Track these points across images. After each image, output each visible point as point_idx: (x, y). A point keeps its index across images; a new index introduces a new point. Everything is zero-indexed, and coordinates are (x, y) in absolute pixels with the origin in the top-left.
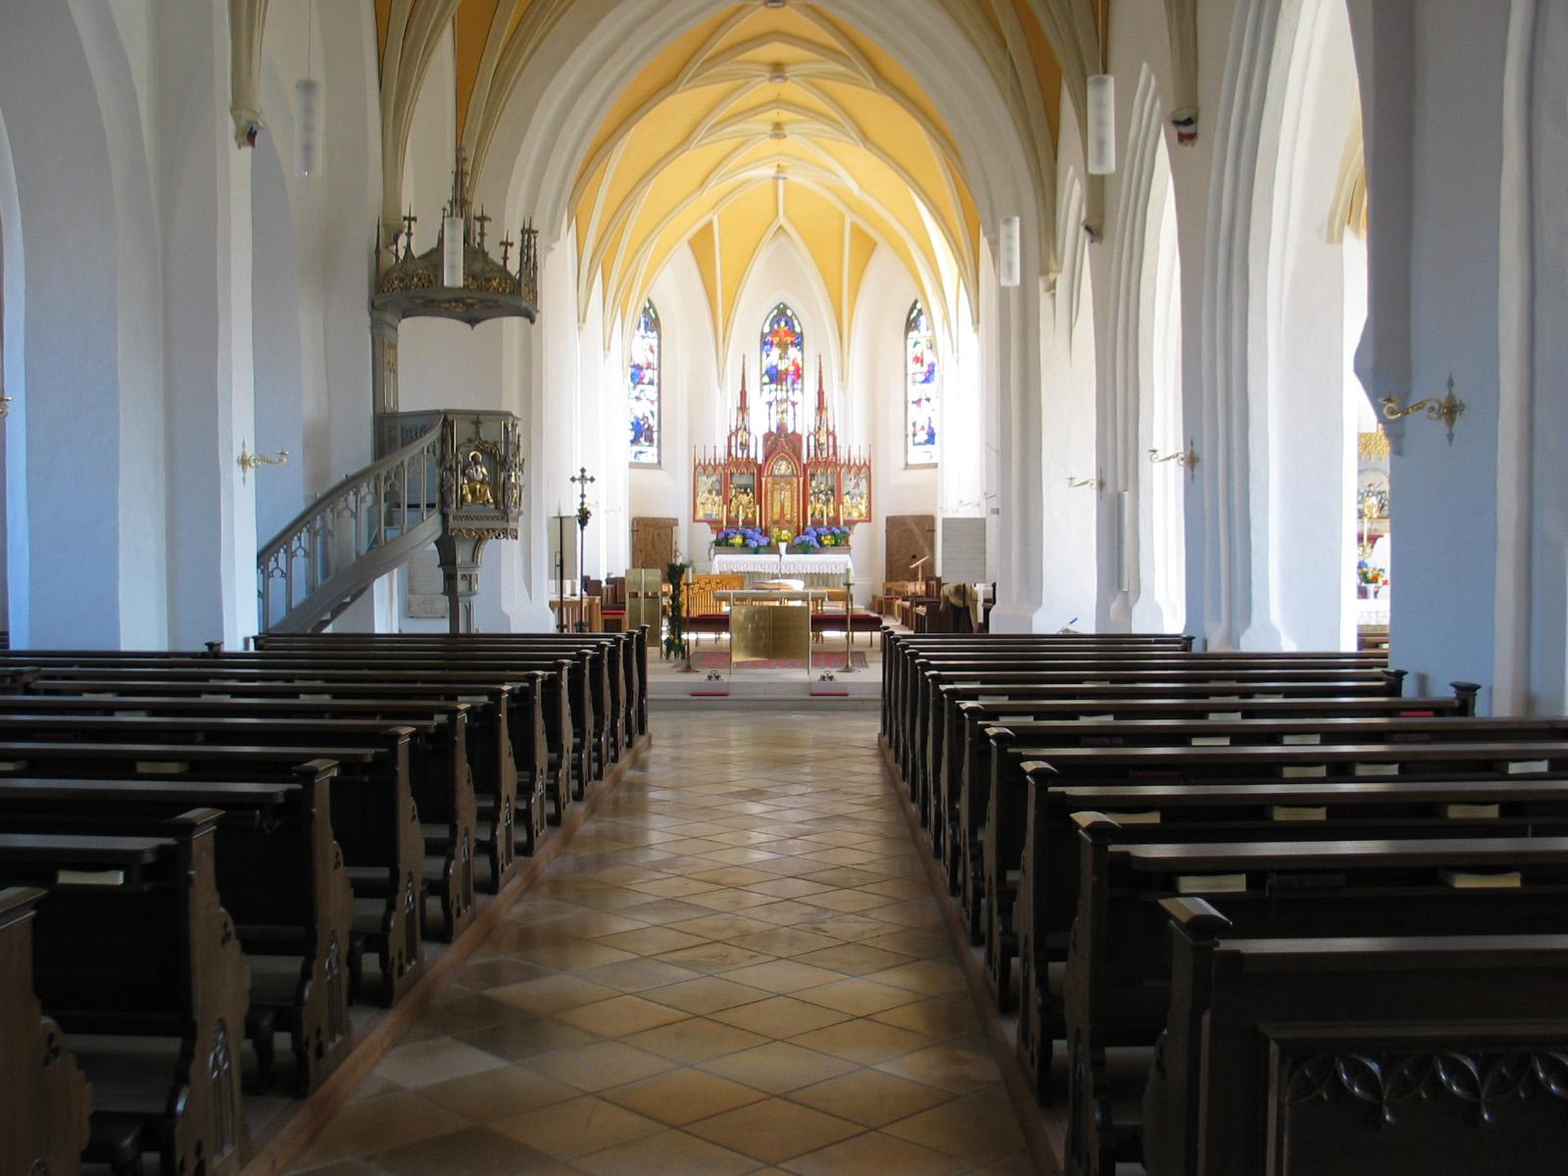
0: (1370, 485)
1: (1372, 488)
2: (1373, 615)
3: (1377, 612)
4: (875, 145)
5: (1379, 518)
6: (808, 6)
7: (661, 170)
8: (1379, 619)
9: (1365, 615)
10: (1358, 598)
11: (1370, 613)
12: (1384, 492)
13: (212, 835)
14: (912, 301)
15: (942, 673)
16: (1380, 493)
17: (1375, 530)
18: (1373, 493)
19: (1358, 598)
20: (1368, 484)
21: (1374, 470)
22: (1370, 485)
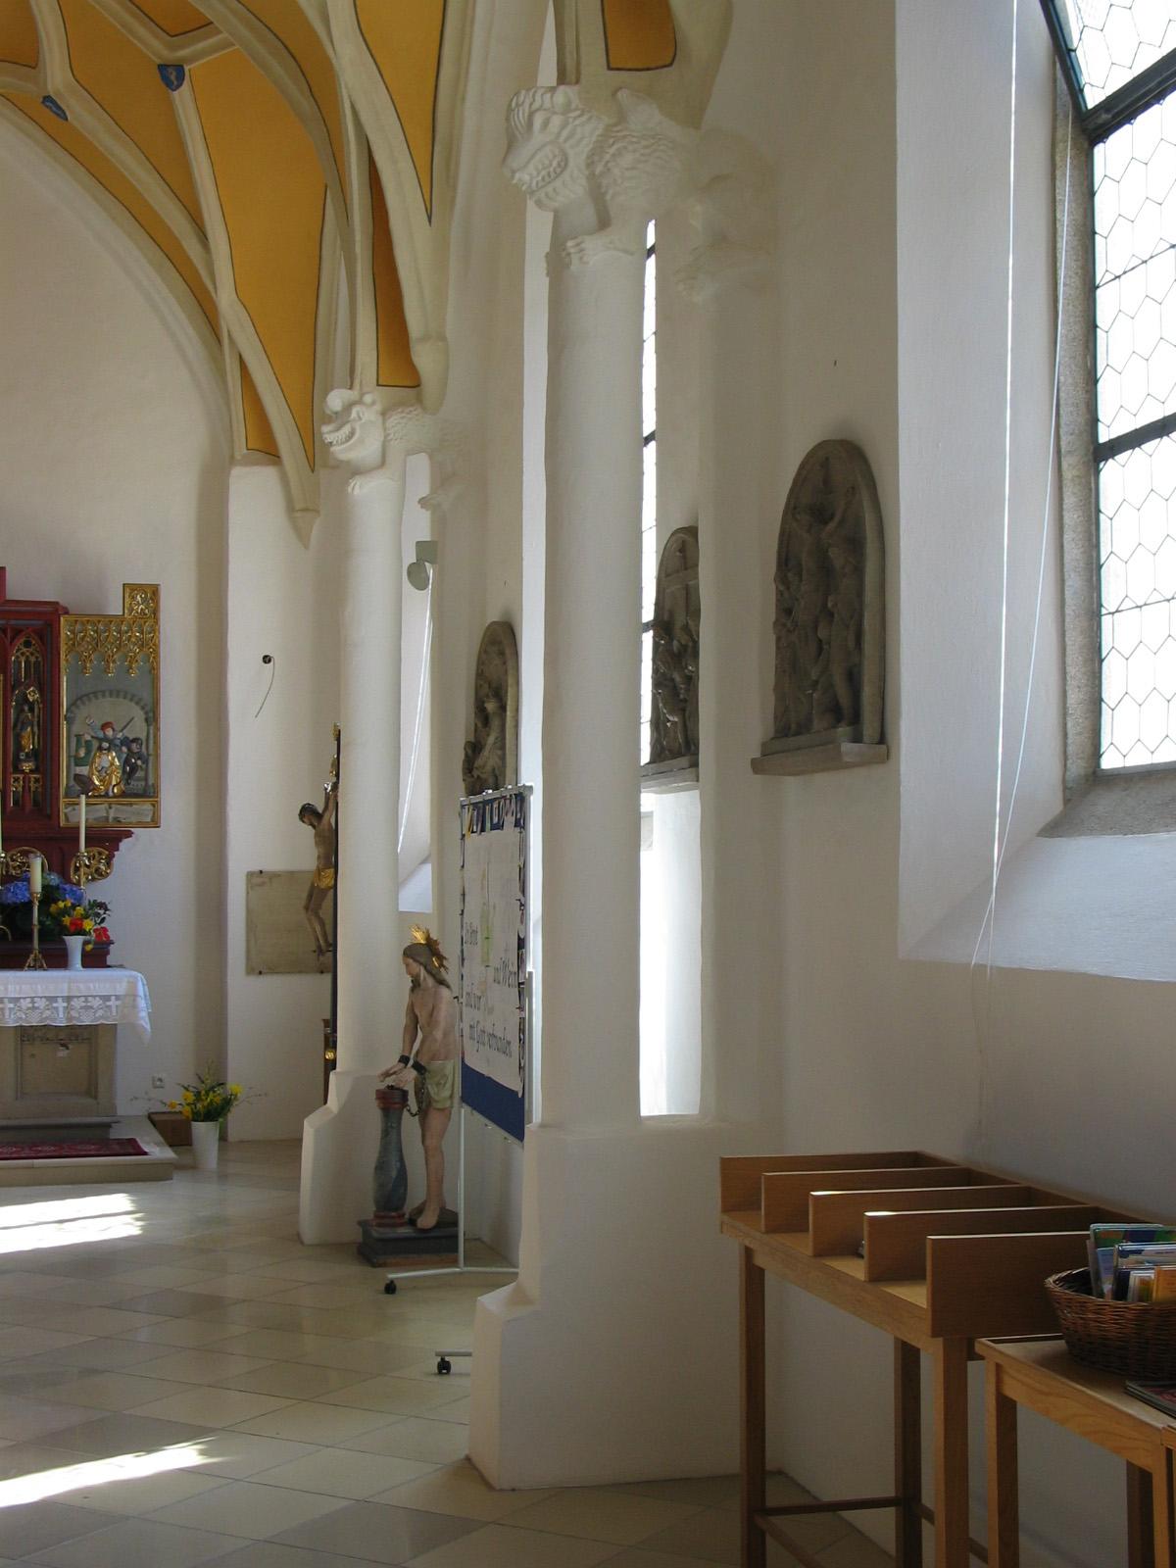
0: (104, 726)
1: (109, 733)
2: (61, 1004)
3: (68, 999)
4: (115, 966)
5: (123, 794)
6: (522, 922)
7: (465, 86)
8: (74, 1014)
9: (41, 1004)
10: (377, 1091)
11: (52, 999)
12: (135, 740)
13: (512, 1082)
14: (700, 779)
15: (648, 614)
16: (126, 742)
17: (117, 820)
18: (110, 741)
19: (377, 1091)
20: (99, 724)
21: (115, 693)
22: (104, 726)
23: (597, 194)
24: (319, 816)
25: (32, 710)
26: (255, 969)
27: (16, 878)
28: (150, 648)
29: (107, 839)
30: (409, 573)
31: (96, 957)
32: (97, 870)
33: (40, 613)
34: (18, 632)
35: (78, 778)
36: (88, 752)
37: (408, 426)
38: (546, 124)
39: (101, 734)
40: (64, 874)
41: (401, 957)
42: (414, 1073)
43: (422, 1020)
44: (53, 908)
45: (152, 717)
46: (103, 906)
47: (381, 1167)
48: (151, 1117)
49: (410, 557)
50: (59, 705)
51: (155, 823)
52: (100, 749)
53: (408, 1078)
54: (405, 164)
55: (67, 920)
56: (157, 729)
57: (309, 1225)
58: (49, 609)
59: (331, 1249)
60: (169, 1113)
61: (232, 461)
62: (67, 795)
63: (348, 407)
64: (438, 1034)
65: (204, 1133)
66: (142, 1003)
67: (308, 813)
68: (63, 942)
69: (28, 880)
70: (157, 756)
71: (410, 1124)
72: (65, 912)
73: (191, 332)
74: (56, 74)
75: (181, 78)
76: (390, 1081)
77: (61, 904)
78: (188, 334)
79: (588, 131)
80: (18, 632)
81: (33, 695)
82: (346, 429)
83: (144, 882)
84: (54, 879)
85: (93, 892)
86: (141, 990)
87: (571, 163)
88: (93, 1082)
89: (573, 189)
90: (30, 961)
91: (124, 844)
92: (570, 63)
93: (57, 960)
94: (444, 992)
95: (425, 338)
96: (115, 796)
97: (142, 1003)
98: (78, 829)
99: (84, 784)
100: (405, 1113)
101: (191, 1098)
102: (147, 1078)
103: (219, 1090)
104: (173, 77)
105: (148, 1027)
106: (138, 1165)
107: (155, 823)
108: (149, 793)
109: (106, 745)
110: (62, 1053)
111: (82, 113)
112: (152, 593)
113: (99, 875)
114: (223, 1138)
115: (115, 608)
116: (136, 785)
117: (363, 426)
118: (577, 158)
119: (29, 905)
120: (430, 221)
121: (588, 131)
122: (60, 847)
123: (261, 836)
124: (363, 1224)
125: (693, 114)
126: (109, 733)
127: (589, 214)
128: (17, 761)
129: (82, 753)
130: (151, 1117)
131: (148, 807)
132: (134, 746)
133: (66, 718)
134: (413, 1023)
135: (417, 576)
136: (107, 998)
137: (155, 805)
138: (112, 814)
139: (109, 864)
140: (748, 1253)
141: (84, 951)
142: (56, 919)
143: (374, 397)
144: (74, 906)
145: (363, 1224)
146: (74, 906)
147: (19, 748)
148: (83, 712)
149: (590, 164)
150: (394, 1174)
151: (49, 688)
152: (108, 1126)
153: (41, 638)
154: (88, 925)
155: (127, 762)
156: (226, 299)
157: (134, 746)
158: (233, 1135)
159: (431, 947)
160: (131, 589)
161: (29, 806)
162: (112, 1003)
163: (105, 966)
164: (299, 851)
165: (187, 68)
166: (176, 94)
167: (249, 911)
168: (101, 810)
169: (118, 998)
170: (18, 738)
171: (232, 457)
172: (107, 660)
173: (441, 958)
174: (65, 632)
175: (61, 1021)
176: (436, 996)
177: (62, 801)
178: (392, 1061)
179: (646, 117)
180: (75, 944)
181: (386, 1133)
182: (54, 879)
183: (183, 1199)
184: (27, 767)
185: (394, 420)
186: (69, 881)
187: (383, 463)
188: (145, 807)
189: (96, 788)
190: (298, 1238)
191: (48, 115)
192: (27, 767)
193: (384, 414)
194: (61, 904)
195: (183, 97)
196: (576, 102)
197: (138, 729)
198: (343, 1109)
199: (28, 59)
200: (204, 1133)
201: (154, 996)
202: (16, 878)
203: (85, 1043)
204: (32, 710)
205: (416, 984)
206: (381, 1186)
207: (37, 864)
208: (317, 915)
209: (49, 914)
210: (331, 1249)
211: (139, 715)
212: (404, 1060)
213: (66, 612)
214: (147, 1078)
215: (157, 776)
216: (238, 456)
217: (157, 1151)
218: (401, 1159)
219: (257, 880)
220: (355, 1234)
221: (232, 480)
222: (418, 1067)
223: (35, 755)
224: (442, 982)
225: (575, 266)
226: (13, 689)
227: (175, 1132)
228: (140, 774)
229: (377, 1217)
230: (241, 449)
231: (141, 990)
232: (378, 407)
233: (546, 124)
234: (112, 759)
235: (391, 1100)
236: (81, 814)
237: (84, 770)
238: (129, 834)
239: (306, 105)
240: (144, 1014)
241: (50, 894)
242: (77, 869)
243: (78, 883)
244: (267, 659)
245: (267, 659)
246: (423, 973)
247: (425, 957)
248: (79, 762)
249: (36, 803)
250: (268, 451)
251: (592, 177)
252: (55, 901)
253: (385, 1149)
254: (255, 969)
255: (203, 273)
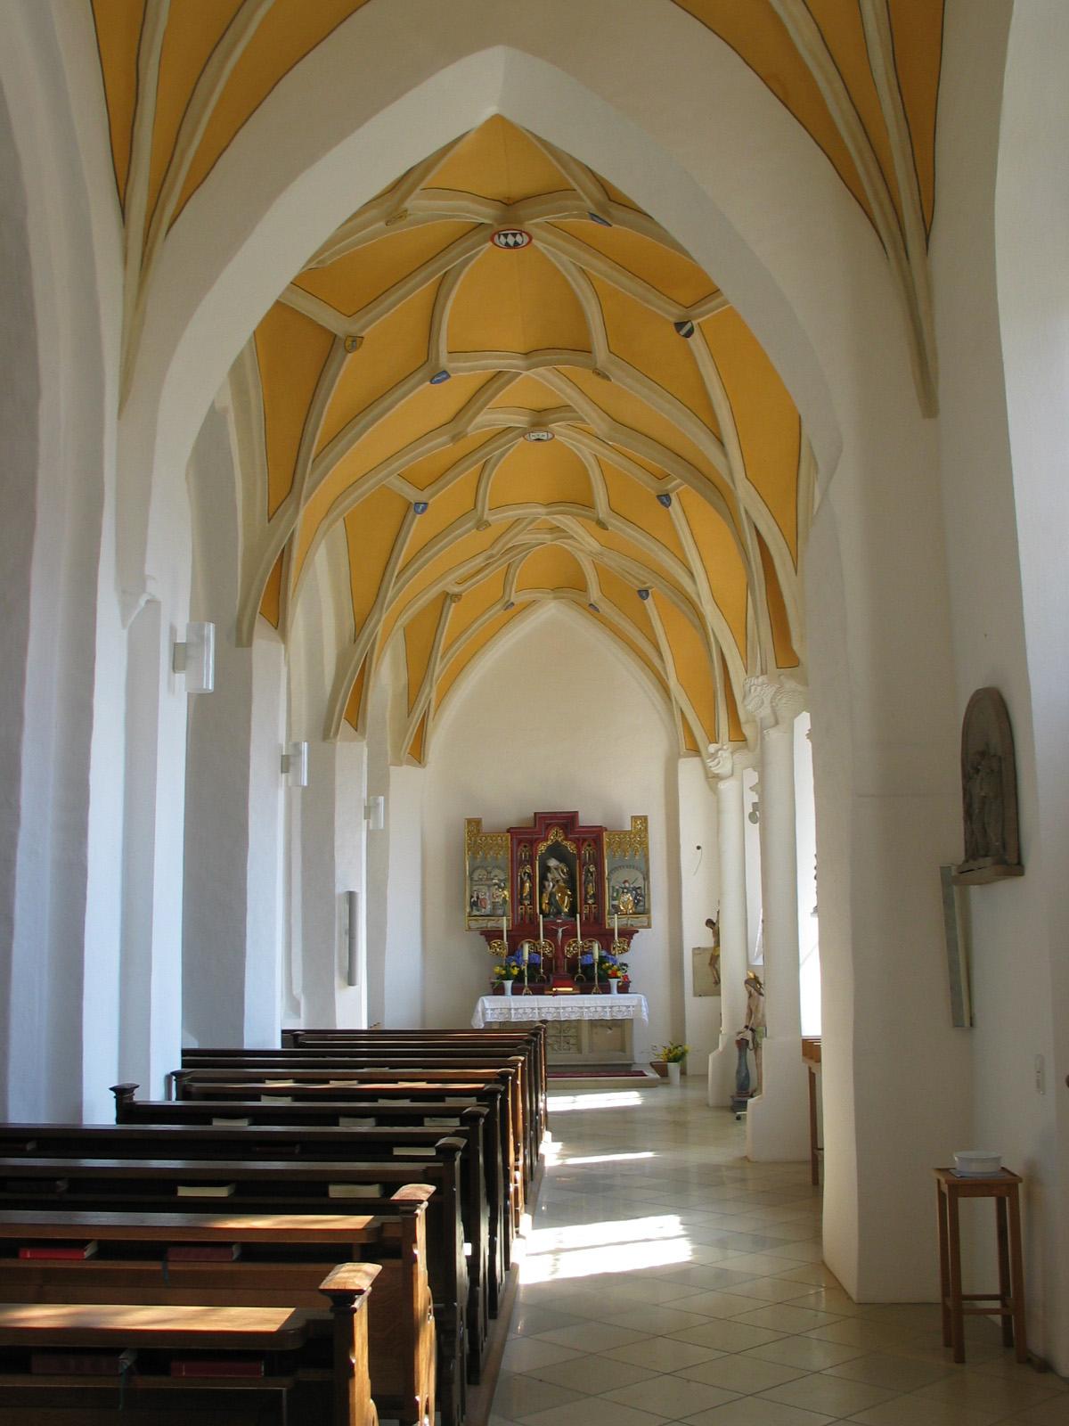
0: (625, 882)
1: (627, 885)
3: (611, 1007)
5: (634, 913)
12: (639, 888)
16: (635, 889)
17: (632, 925)
20: (623, 880)
22: (625, 882)
23: (774, 712)
24: (714, 924)
25: (592, 875)
26: (698, 994)
27: (587, 953)
28: (644, 844)
29: (627, 934)
30: (750, 817)
31: (623, 989)
32: (624, 949)
33: (594, 831)
34: (584, 840)
35: (613, 906)
36: (617, 895)
37: (743, 757)
38: (755, 690)
39: (623, 886)
40: (609, 951)
41: (743, 983)
42: (750, 1032)
43: (753, 1009)
44: (604, 966)
45: (646, 877)
46: (625, 965)
47: (738, 1072)
48: (651, 1064)
49: (749, 809)
50: (604, 872)
51: (649, 926)
52: (623, 892)
53: (748, 1035)
54: (735, 650)
55: (610, 972)
56: (649, 882)
57: (711, 1102)
58: (598, 829)
59: (720, 1108)
60: (512, 851)
61: (679, 756)
62: (609, 914)
63: (717, 751)
64: (760, 1016)
65: (674, 1068)
66: (644, 1009)
67: (710, 923)
68: (608, 981)
69: (592, 954)
70: (649, 895)
71: (750, 1054)
72: (609, 968)
73: (657, 695)
74: (595, 594)
75: (648, 595)
76: (741, 1036)
77: (607, 964)
78: (657, 697)
79: (770, 691)
80: (584, 840)
81: (592, 869)
82: (717, 760)
83: (645, 955)
84: (604, 953)
85: (621, 959)
86: (644, 1003)
87: (765, 702)
88: (623, 1046)
89: (766, 712)
90: (594, 991)
91: (636, 936)
92: (764, 667)
93: (606, 990)
94: (762, 998)
95: (746, 722)
96: (630, 914)
97: (644, 1009)
98: (613, 930)
99: (616, 909)
100: (748, 1050)
101: (667, 1051)
102: (647, 1046)
103: (680, 1048)
104: (665, 500)
105: (647, 1019)
106: (640, 1081)
107: (649, 926)
108: (646, 912)
109: (625, 890)
110: (610, 1032)
111: (606, 608)
112: (644, 819)
113: (625, 951)
114: (683, 1073)
115: (628, 827)
116: (640, 909)
117: (725, 758)
118: (767, 703)
119: (593, 965)
120: (747, 672)
121: (770, 691)
122: (606, 938)
123: (695, 936)
124: (732, 1097)
125: (804, 681)
126: (627, 885)
127: (772, 720)
128: (586, 899)
129: (615, 895)
130: (651, 1064)
131: (645, 919)
132: (638, 891)
133: (608, 879)
134: (751, 1013)
135: (753, 818)
136: (628, 1007)
137: (649, 918)
138: (629, 922)
139: (628, 946)
140: (810, 1069)
141: (618, 987)
142: (605, 971)
143: (728, 746)
144: (613, 965)
145: (732, 1097)
146: (613, 965)
147: (587, 893)
148: (614, 876)
149: (771, 702)
150: (744, 1075)
151: (599, 863)
152: (630, 1065)
153: (595, 843)
154: (619, 974)
155: (635, 898)
156: (673, 683)
157: (638, 891)
158: (689, 1071)
159: (756, 979)
160: (634, 818)
161: (592, 920)
162: (631, 1009)
163: (627, 993)
164: (704, 938)
165: (650, 591)
166: (645, 601)
167: (694, 967)
168: (624, 921)
169: (633, 1006)
170: (586, 888)
171: (679, 753)
172: (624, 851)
173: (760, 984)
174: (606, 840)
175: (608, 1017)
176: (759, 999)
177: (607, 917)
178: (742, 1028)
179: (790, 685)
180: (614, 982)
181: (740, 1058)
182: (604, 953)
183: (662, 1096)
184: (590, 902)
185: (737, 755)
186: (610, 954)
187: (732, 775)
188: (643, 918)
189: (622, 911)
190: (708, 1105)
191: (591, 609)
192: (590, 902)
193: (732, 753)
194: (607, 964)
195: (649, 602)
196: (766, 682)
197: (640, 883)
198: (724, 1048)
199: (582, 588)
200: (674, 1068)
201: (649, 1006)
202: (587, 953)
203: (619, 1027)
204: (592, 875)
205: (750, 995)
206: (738, 1079)
207: (596, 946)
208: (714, 967)
209: (602, 969)
210: (720, 1108)
211: (641, 876)
212: (747, 1027)
213: (606, 830)
214: (647, 1046)
215: (649, 905)
216: (682, 753)
217: (652, 1075)
218: (747, 1069)
219: (696, 952)
220: (729, 1102)
221: (679, 765)
222: (752, 1030)
223: (594, 896)
224: (761, 994)
225: (767, 739)
226: (583, 866)
227: (662, 1070)
228: (641, 903)
229: (738, 1093)
230: (683, 750)
231: (644, 1003)
232: (730, 750)
233: (755, 690)
234: (628, 897)
235: (742, 1044)
236: (615, 923)
237: (616, 903)
238: (637, 932)
239: (697, 622)
240: (645, 1014)
241: (602, 960)
242: (614, 948)
243: (615, 955)
244: (699, 848)
245: (699, 848)
246: (753, 990)
247: (754, 984)
248: (614, 899)
249: (595, 918)
250: (695, 750)
251: (772, 707)
252: (605, 963)
253: (740, 1065)
254: (698, 994)
255: (662, 673)
